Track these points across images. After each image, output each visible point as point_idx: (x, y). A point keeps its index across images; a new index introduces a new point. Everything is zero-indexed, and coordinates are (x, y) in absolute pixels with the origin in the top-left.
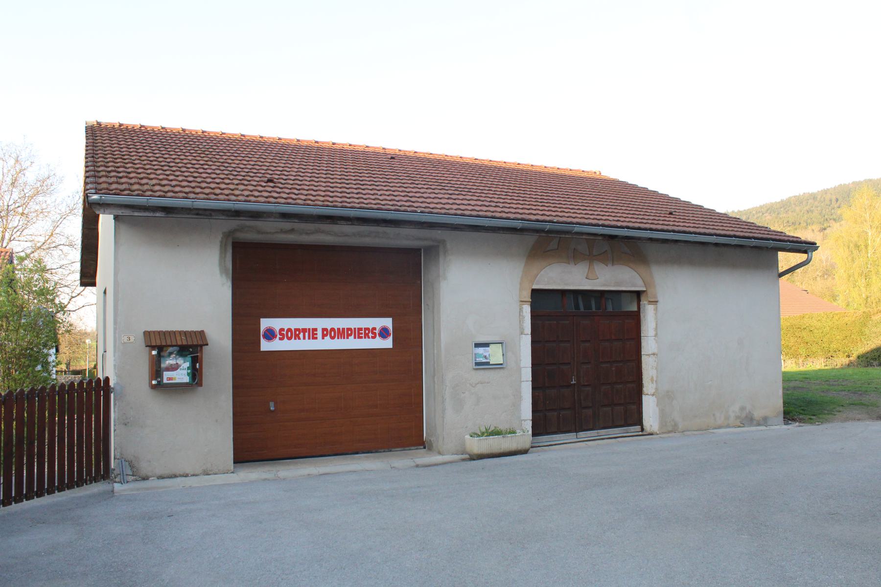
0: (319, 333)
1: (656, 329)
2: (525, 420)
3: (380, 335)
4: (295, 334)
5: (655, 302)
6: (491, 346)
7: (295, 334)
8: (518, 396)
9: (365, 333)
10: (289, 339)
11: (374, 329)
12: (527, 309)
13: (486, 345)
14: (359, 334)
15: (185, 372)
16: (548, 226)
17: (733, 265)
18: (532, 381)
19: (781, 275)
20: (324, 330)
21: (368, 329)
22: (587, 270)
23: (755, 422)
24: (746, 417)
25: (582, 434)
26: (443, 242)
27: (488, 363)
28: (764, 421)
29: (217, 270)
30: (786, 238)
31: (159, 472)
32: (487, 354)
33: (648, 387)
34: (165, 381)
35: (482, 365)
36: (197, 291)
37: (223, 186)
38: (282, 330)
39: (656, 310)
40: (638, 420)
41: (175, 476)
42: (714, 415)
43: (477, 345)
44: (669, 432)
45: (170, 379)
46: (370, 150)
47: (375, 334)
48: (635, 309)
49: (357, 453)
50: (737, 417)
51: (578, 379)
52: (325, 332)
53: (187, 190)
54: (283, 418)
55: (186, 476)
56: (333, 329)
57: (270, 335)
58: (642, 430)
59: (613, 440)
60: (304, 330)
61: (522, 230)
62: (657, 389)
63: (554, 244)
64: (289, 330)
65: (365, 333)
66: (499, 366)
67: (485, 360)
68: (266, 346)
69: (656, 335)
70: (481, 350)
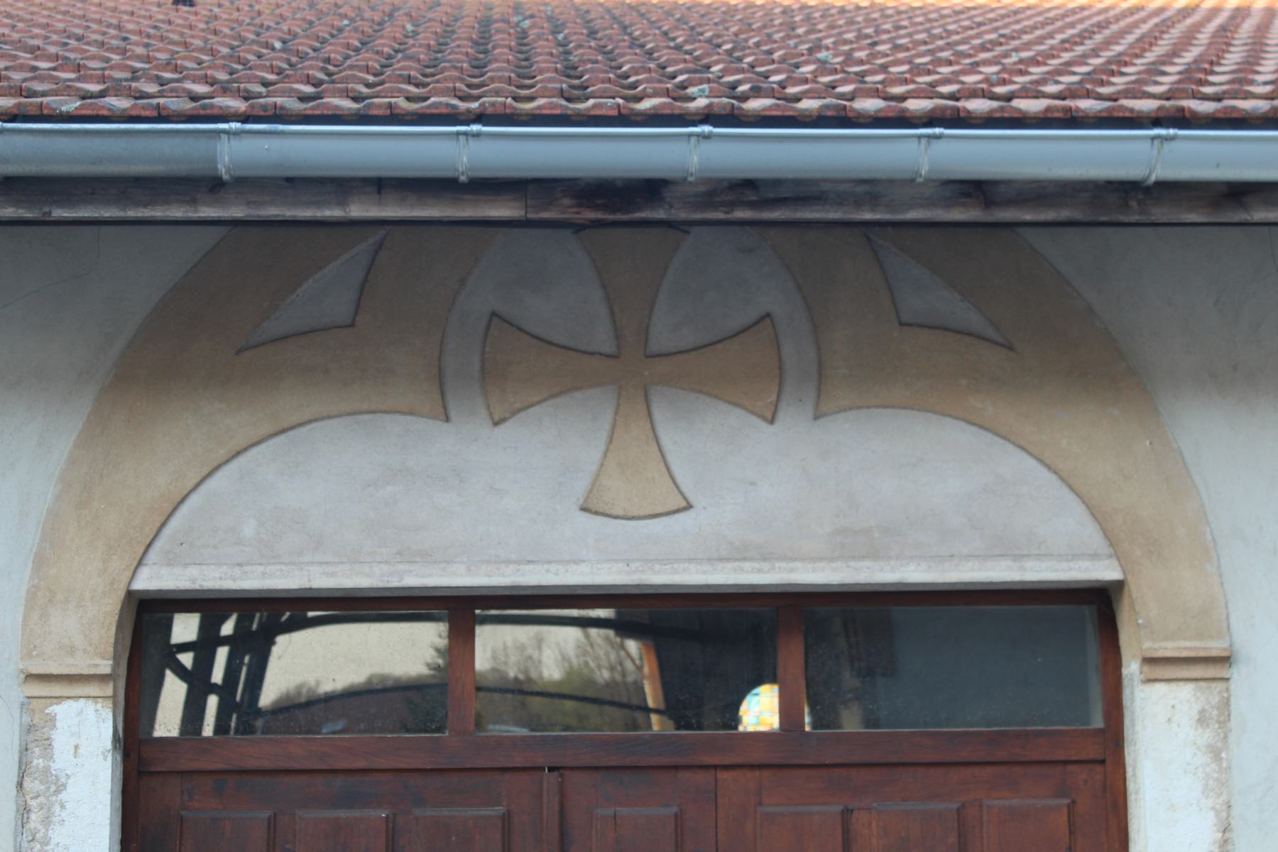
5: (1214, 664)
39: (1220, 718)
48: (1098, 722)
63: (328, 290)
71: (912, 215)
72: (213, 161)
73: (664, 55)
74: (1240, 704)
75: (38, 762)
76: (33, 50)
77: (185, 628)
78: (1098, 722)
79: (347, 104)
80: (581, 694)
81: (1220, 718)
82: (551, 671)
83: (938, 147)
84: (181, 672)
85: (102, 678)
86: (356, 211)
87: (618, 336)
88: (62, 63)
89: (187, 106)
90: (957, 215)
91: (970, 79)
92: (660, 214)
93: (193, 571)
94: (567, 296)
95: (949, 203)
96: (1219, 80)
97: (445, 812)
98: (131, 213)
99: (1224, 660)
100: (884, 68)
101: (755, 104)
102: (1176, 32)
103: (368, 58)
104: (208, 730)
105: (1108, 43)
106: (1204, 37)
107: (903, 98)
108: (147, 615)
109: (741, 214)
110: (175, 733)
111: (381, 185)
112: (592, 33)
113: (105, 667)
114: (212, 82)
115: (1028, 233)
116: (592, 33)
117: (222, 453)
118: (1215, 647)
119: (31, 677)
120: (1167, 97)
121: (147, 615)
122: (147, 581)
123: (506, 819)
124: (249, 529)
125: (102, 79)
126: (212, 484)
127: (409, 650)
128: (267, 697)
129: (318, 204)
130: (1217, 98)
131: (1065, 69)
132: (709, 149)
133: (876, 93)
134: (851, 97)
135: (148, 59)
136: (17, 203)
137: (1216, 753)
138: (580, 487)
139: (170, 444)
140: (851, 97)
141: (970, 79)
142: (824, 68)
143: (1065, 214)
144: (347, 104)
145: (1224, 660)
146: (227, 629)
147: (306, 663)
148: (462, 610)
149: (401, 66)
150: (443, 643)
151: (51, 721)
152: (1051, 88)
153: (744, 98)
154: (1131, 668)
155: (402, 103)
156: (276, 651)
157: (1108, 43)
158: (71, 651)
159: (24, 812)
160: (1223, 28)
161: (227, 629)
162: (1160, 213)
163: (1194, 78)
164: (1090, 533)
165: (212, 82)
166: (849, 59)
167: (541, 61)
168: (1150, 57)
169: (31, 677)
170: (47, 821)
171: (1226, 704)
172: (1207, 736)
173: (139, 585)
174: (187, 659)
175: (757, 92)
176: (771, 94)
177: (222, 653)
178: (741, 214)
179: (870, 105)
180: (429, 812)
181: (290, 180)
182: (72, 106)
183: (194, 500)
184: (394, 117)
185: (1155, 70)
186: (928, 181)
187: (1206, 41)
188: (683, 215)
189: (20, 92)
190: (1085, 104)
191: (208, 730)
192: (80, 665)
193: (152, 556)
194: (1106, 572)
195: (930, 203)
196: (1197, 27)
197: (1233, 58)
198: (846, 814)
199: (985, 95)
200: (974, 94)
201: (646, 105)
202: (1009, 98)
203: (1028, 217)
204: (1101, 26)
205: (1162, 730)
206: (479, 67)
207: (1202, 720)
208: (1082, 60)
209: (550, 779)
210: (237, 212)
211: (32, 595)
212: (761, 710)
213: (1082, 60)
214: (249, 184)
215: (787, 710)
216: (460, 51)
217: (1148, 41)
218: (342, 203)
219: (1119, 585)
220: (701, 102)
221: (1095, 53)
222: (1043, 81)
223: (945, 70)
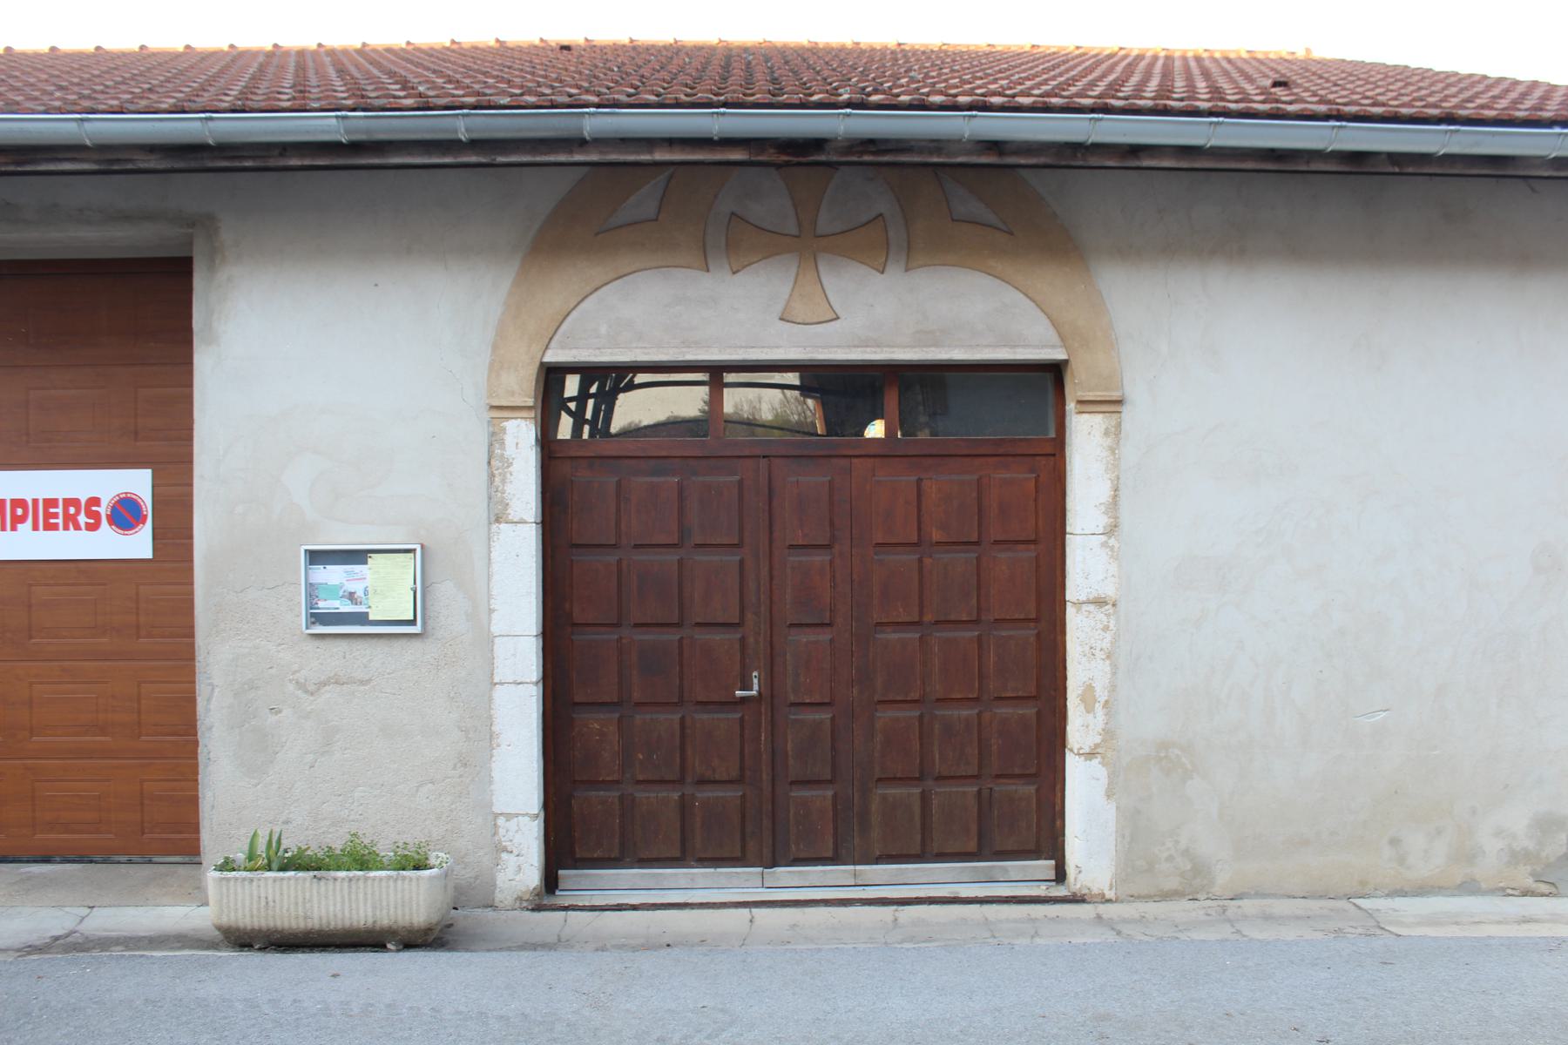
1: (1114, 504)
2: (509, 817)
3: (112, 520)
5: (1114, 404)
6: (374, 560)
7: (69, 514)
8: (481, 734)
11: (95, 501)
12: (522, 437)
13: (356, 557)
14: (48, 516)
16: (462, 126)
17: (1298, 249)
21: (75, 502)
22: (786, 290)
25: (790, 880)
27: (362, 619)
32: (358, 588)
33: (1081, 728)
39: (1115, 433)
40: (1044, 837)
42: (1394, 842)
43: (315, 557)
44: (1166, 896)
47: (96, 516)
48: (1052, 435)
50: (1516, 857)
51: (770, 680)
58: (1061, 876)
62: (1108, 734)
63: (643, 201)
69: (1112, 530)
70: (332, 575)
71: (960, 160)
72: (581, 129)
73: (826, 73)
74: (1126, 426)
75: (498, 451)
76: (484, 74)
77: (572, 385)
78: (1052, 435)
79: (653, 98)
80: (780, 426)
81: (1115, 433)
82: (767, 415)
83: (975, 122)
84: (569, 412)
85: (529, 408)
86: (660, 156)
87: (800, 225)
88: (500, 79)
89: (566, 100)
90: (984, 160)
91: (992, 87)
92: (823, 158)
93: (574, 352)
94: (772, 202)
95: (980, 153)
96: (1127, 89)
97: (708, 479)
98: (539, 159)
99: (1119, 402)
100: (946, 81)
101: (874, 98)
102: (1104, 66)
103: (664, 74)
104: (586, 436)
105: (1067, 71)
106: (1119, 69)
107: (956, 96)
108: (552, 376)
109: (867, 158)
110: (568, 437)
111: (672, 142)
112: (787, 63)
113: (530, 402)
114: (579, 87)
115: (1023, 172)
116: (787, 63)
117: (588, 289)
118: (1115, 395)
119: (493, 407)
120: (1099, 97)
121: (552, 376)
122: (550, 357)
123: (741, 482)
124: (603, 330)
125: (522, 87)
126: (583, 305)
127: (688, 402)
128: (614, 428)
129: (638, 153)
130: (1126, 98)
131: (1045, 82)
132: (849, 121)
133: (941, 93)
134: (928, 95)
135: (546, 77)
136: (477, 154)
137: (1112, 450)
138: (779, 308)
139: (559, 286)
140: (928, 95)
141: (992, 87)
142: (912, 80)
143: (1042, 160)
144: (653, 98)
145: (1119, 402)
146: (593, 390)
147: (635, 409)
148: (716, 374)
149: (681, 78)
150: (707, 398)
151: (504, 430)
152: (1036, 92)
153: (869, 95)
154: (1071, 406)
155: (683, 97)
156: (618, 403)
157: (1067, 71)
158: (513, 393)
159: (492, 476)
160: (1130, 64)
161: (593, 390)
162: (1094, 161)
163: (1114, 88)
164: (1055, 339)
165: (579, 87)
166: (927, 76)
167: (759, 76)
168: (1090, 78)
169: (493, 407)
170: (503, 481)
171: (1119, 425)
172: (1109, 441)
173: (547, 359)
174: (572, 406)
175: (876, 91)
176: (884, 92)
177: (591, 402)
178: (867, 158)
179: (937, 99)
180: (701, 479)
181: (623, 140)
182: (505, 100)
183: (574, 314)
184: (678, 105)
185: (1092, 84)
186: (969, 141)
187: (499, 693)
188: (835, 159)
189: (478, 94)
190: (1054, 100)
191: (586, 436)
193: (553, 344)
194: (1059, 355)
195: (969, 153)
196: (1116, 64)
197: (1134, 80)
198: (920, 481)
199: (1000, 94)
200: (994, 94)
201: (815, 98)
202: (1014, 96)
203: (1023, 161)
204: (1064, 62)
206: (725, 79)
207: (1106, 433)
208: (1054, 78)
209: (763, 462)
210: (594, 157)
211: (491, 365)
212: (876, 430)
213: (1054, 78)
214: (600, 142)
215: (889, 430)
216: (714, 71)
217: (1089, 70)
218: (651, 152)
219: (1066, 362)
220: (846, 96)
221: (1061, 75)
222: (1032, 88)
223: (979, 82)
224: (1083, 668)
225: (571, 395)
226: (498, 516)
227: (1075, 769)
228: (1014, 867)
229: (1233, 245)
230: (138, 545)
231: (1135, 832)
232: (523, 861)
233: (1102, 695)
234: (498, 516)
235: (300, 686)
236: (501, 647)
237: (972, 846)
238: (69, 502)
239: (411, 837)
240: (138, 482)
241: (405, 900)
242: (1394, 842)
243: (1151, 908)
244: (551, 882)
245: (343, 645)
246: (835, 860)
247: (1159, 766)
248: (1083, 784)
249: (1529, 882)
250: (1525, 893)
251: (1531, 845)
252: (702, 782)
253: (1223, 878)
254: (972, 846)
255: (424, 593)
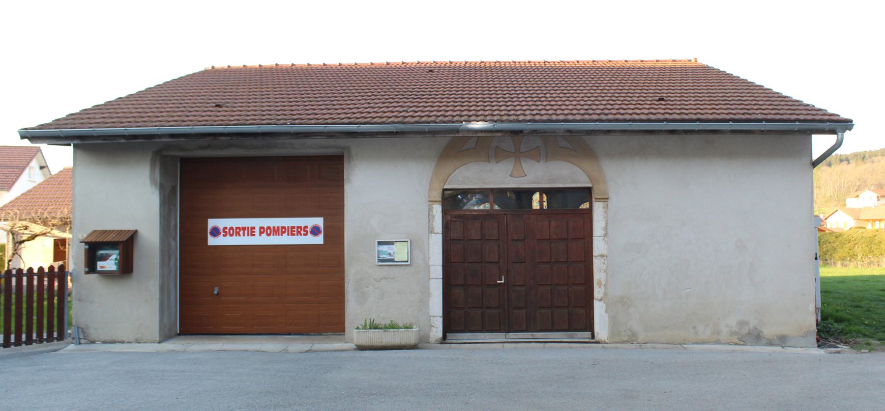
0: (257, 231)
1: (606, 228)
2: (434, 317)
3: (312, 233)
4: (237, 231)
5: (605, 199)
6: (396, 244)
7: (237, 231)
9: (298, 231)
10: (231, 235)
11: (306, 227)
12: (438, 209)
13: (392, 243)
15: (113, 262)
17: (662, 154)
18: (443, 278)
19: (815, 164)
20: (261, 228)
21: (300, 227)
22: (512, 168)
23: (764, 341)
24: (749, 333)
25: (513, 336)
26: (348, 149)
27: (393, 260)
28: (782, 340)
29: (148, 181)
30: (826, 118)
31: (103, 338)
32: (392, 252)
33: (598, 292)
34: (99, 269)
35: (387, 262)
36: (133, 201)
37: (579, 107)
38: (226, 228)
39: (606, 207)
40: (588, 325)
41: (114, 342)
42: (694, 328)
43: (380, 243)
44: (624, 342)
45: (102, 267)
46: (679, 65)
47: (307, 231)
49: (289, 334)
50: (732, 333)
51: (507, 279)
52: (262, 230)
53: (550, 112)
54: (208, 299)
55: (123, 342)
56: (269, 228)
57: (216, 232)
58: (593, 337)
59: (542, 345)
60: (244, 229)
61: (434, 133)
62: (605, 294)
64: (231, 228)
65: (298, 231)
66: (403, 264)
67: (389, 257)
68: (212, 241)
69: (605, 235)
70: (384, 248)
74: (610, 205)
94: (508, 143)
138: (509, 173)
164: (587, 179)
187: (432, 281)
192: (437, 199)
194: (590, 185)
205: (598, 209)
224: (598, 275)
225: (452, 201)
226: (431, 231)
227: (596, 304)
228: (579, 334)
229: (641, 153)
230: (319, 240)
231: (614, 323)
232: (437, 331)
233: (603, 283)
234: (431, 231)
235: (375, 279)
236: (432, 268)
237: (566, 328)
238: (298, 227)
239: (408, 321)
240: (319, 221)
241: (409, 337)
242: (694, 328)
243: (619, 345)
244: (444, 337)
245: (387, 268)
246: (526, 331)
247: (620, 304)
248: (599, 309)
249: (737, 341)
250: (736, 344)
251: (737, 330)
252: (488, 308)
253: (641, 337)
254: (566, 328)
255: (411, 252)
